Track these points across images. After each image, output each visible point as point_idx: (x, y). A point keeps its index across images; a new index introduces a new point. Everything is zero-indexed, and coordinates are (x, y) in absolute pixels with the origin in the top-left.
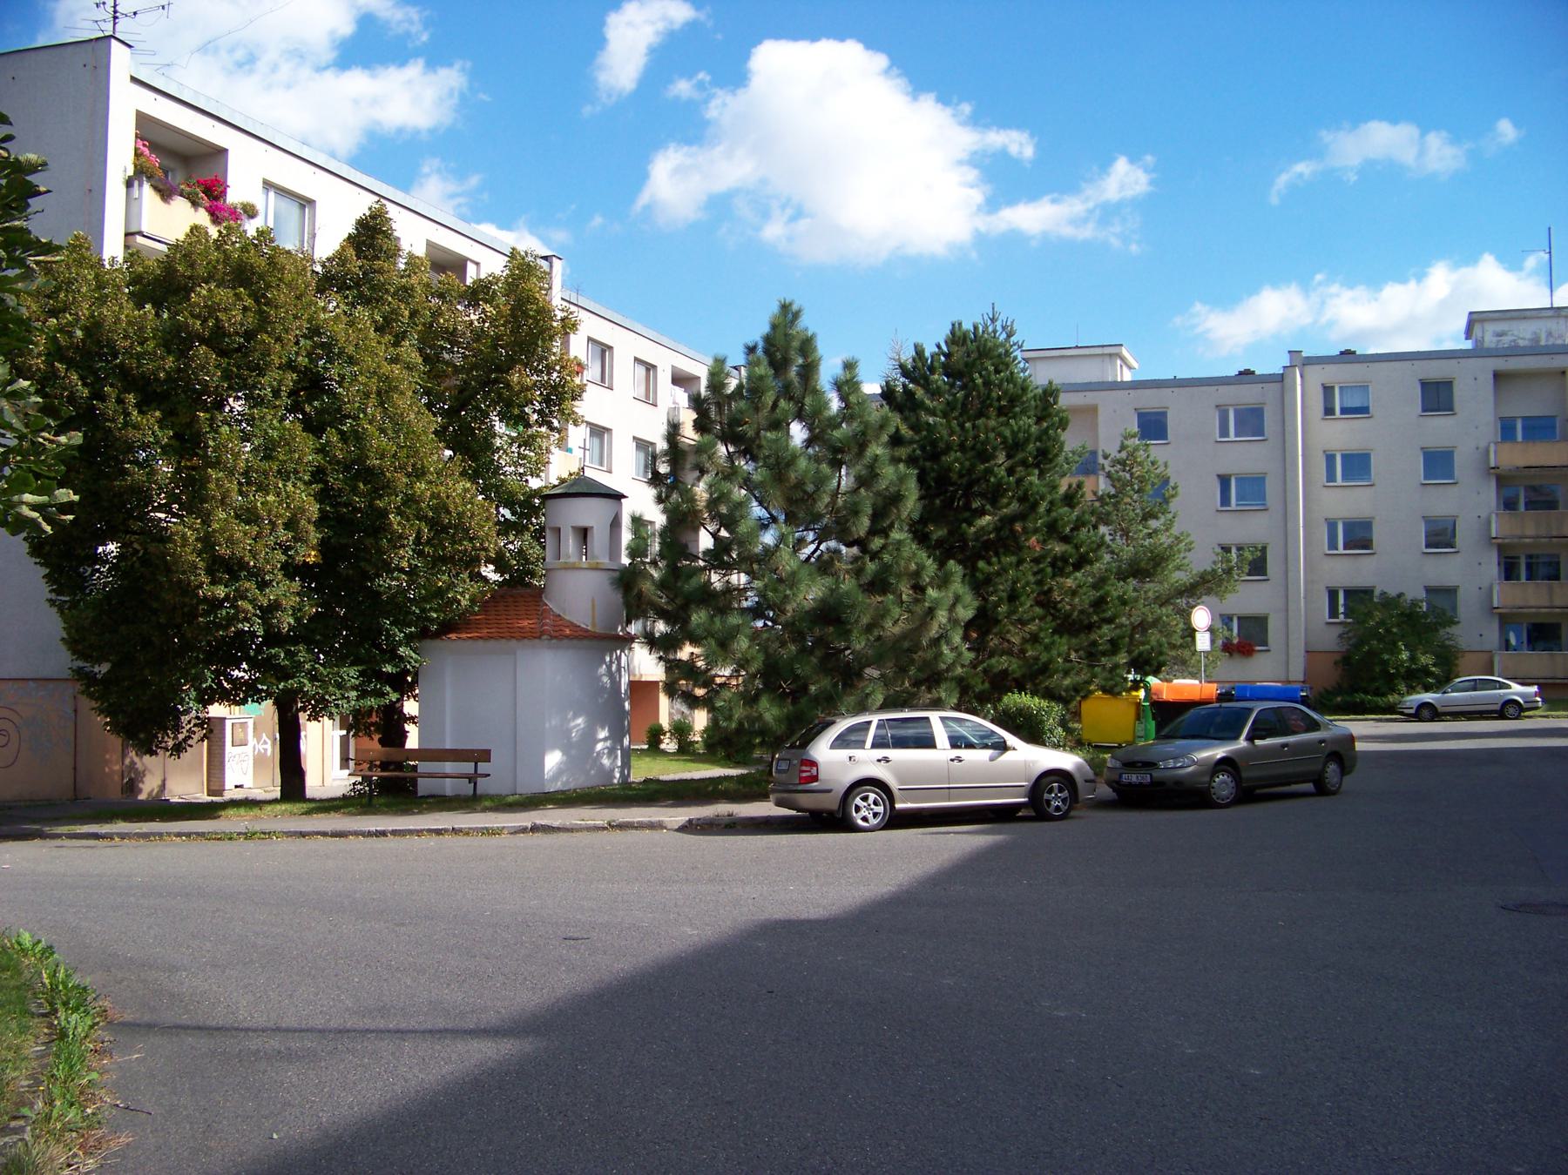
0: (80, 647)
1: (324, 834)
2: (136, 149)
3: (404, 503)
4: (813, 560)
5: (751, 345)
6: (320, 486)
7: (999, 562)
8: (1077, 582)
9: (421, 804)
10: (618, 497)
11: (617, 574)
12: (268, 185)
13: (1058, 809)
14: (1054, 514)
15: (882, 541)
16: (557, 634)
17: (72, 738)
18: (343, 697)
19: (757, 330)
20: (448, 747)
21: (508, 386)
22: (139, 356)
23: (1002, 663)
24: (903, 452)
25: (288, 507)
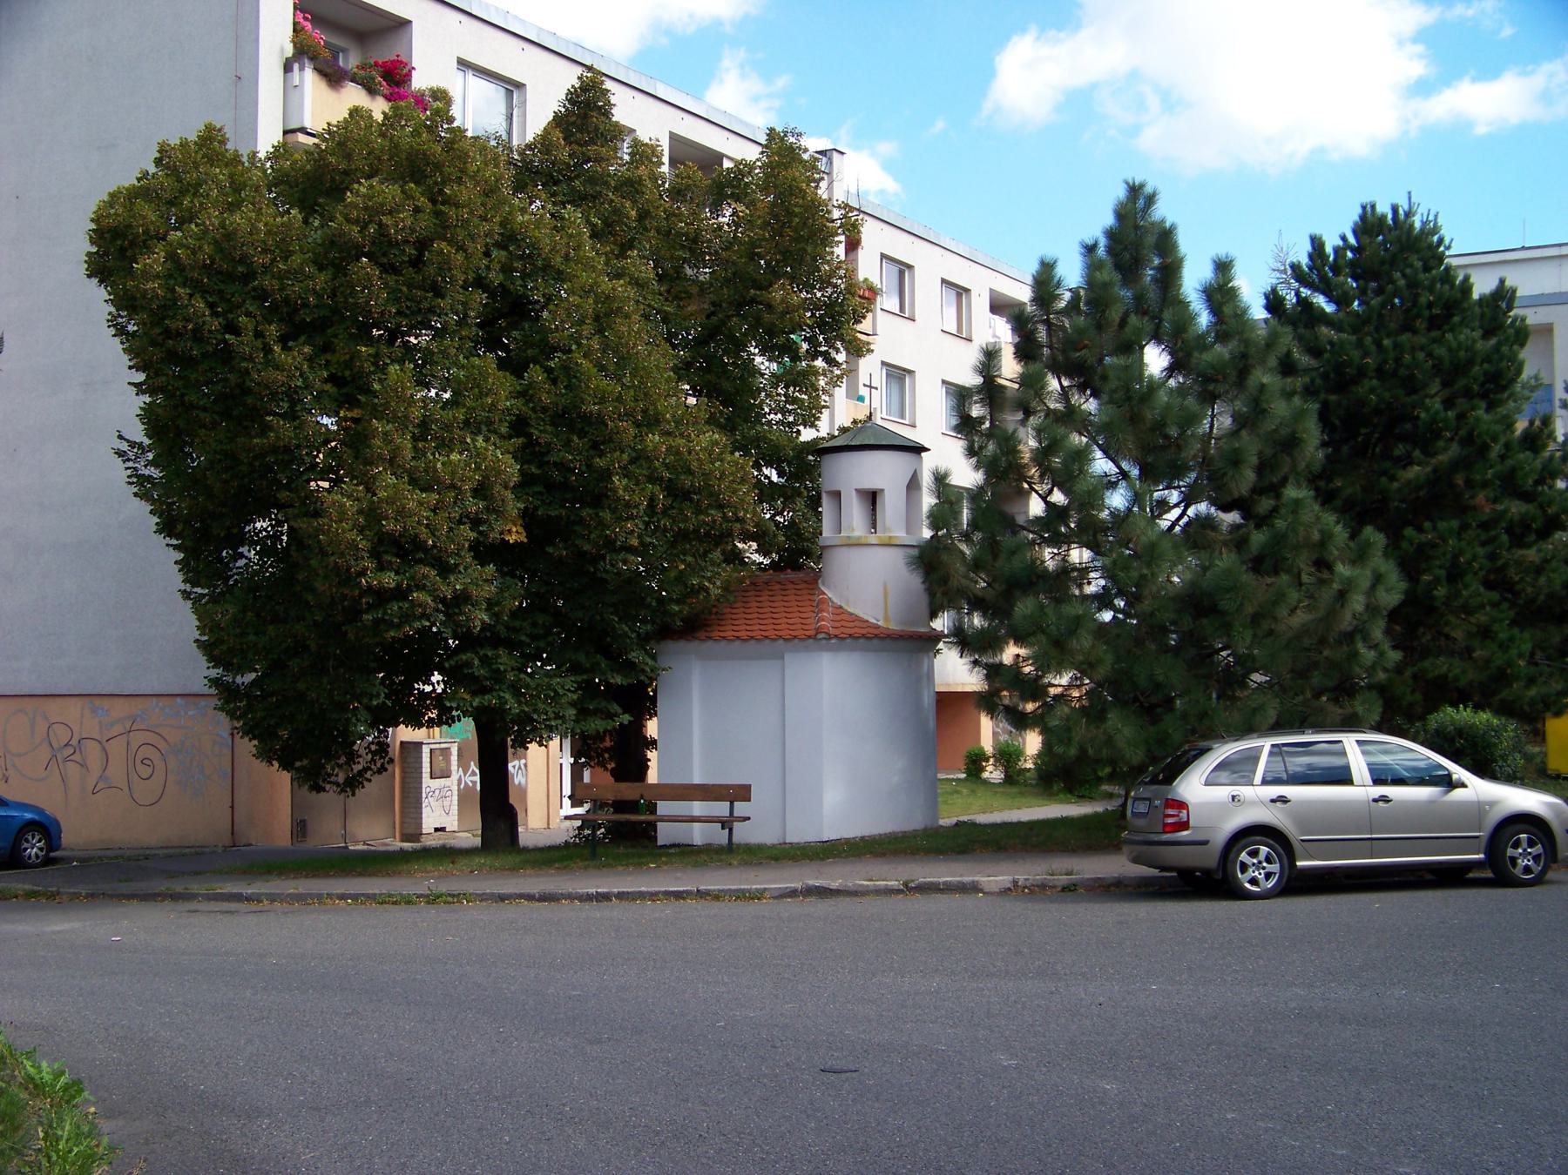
0: (216, 652)
1: (530, 897)
2: (295, 24)
3: (633, 461)
4: (1177, 528)
5: (1090, 242)
6: (521, 440)
7: (1434, 528)
8: (1542, 555)
9: (660, 856)
10: (918, 450)
11: (915, 552)
12: (463, 64)
13: (1527, 870)
14: (1510, 462)
15: (1272, 502)
16: (837, 632)
17: (229, 770)
18: (557, 717)
19: (1097, 221)
20: (697, 781)
21: (769, 307)
22: (281, 276)
23: (1440, 666)
24: (1299, 382)
25: (478, 468)
